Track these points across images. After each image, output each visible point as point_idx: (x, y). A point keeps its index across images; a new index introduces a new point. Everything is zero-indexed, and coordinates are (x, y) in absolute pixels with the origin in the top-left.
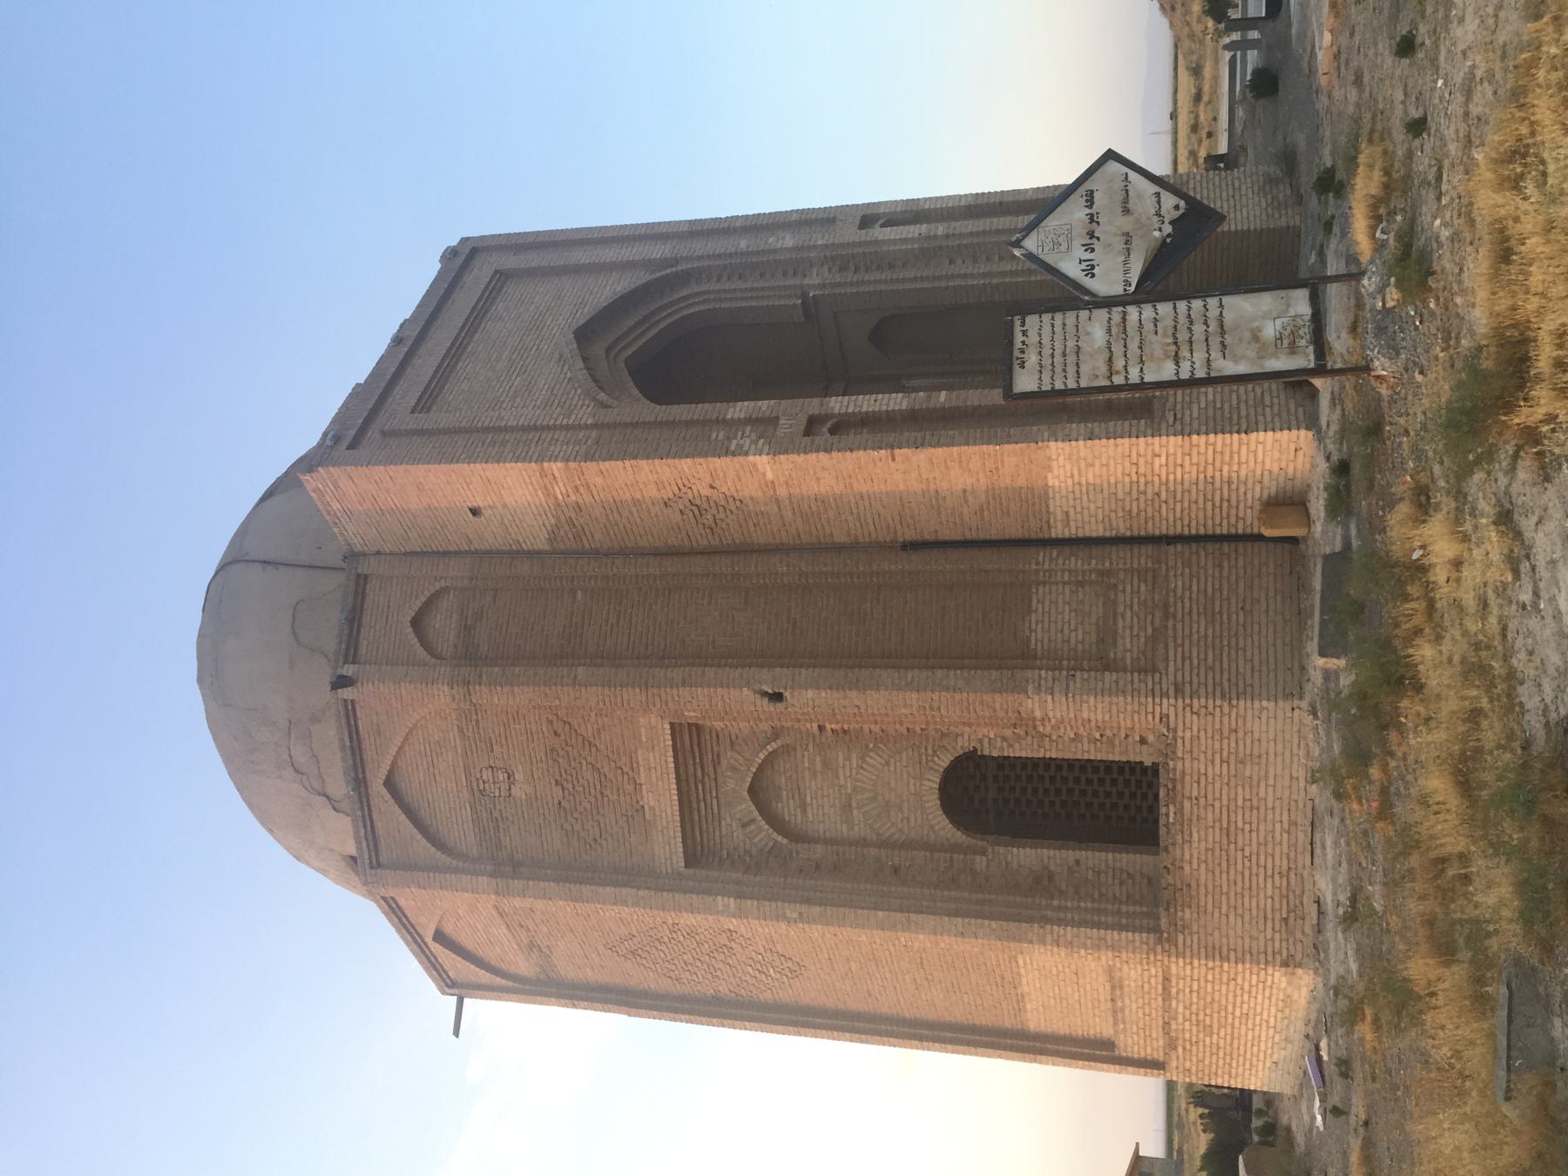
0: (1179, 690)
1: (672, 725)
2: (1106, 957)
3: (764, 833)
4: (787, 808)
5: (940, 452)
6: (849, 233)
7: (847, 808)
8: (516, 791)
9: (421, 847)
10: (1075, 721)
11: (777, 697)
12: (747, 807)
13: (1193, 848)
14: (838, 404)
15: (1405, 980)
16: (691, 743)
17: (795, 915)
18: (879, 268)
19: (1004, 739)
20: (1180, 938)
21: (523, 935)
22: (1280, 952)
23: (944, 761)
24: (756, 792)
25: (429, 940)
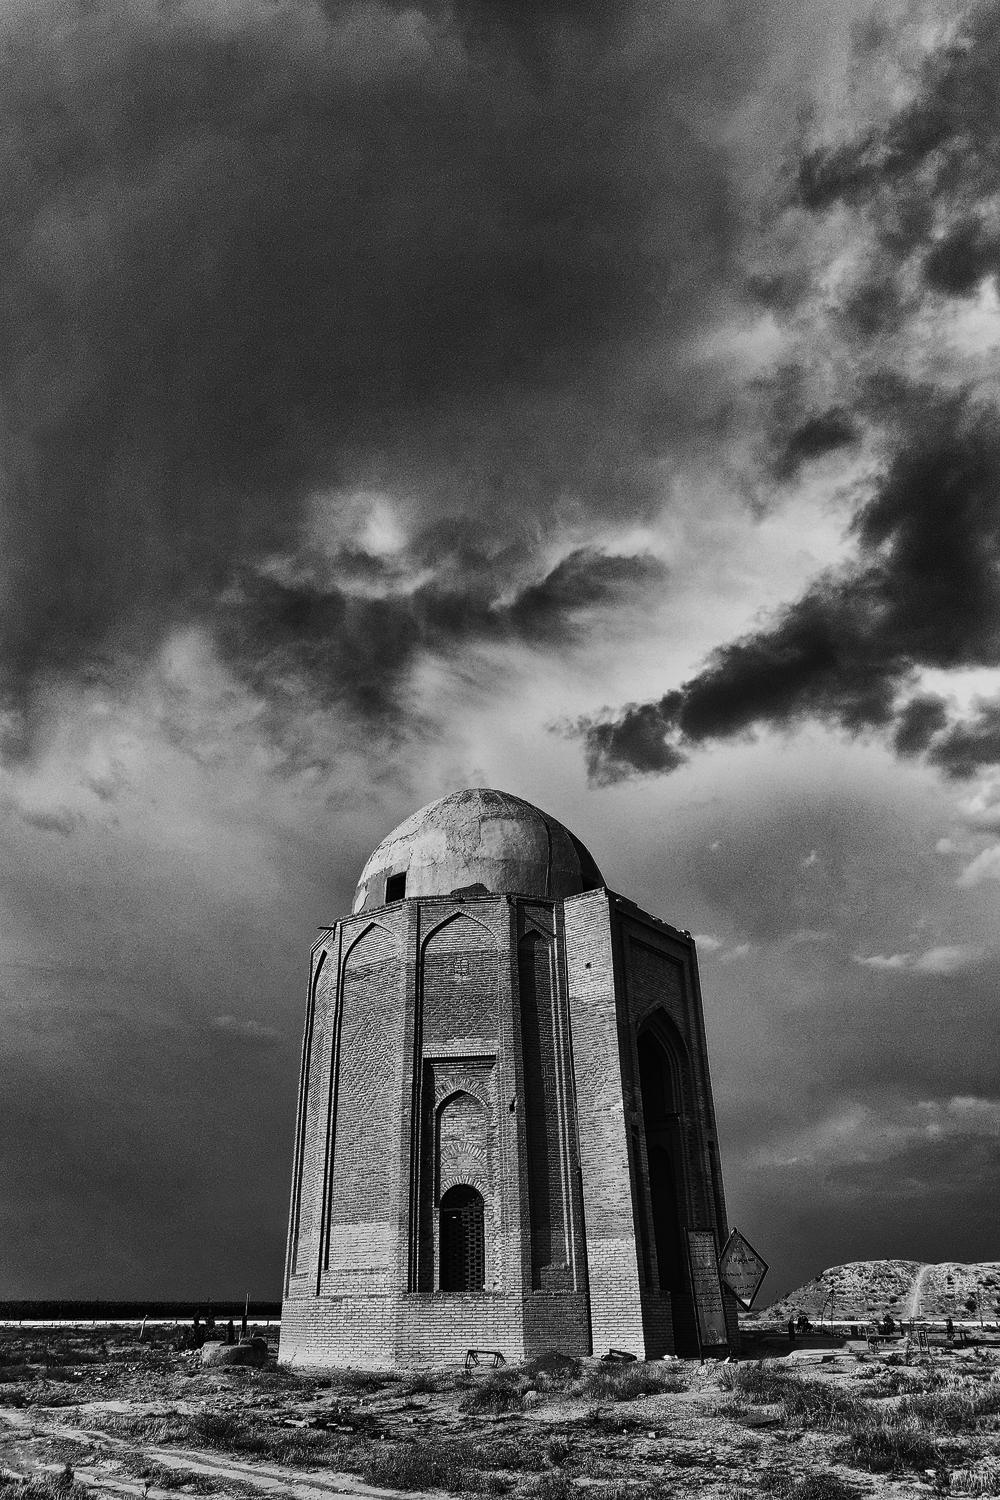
0: (524, 1301)
1: (493, 1057)
2: (394, 1266)
3: (440, 1098)
4: (451, 1108)
5: (628, 1188)
6: (706, 1137)
7: (453, 1138)
8: (457, 976)
9: (427, 929)
10: (503, 1252)
11: (512, 1108)
12: (452, 1089)
13: (449, 1307)
14: (643, 1139)
15: (921, 386)
16: (488, 1061)
17: (406, 1113)
18: (691, 1152)
19: (493, 1217)
20: (407, 1302)
21: (378, 968)
22: (403, 1351)
23: (479, 1187)
24: (459, 1094)
25: (372, 921)
